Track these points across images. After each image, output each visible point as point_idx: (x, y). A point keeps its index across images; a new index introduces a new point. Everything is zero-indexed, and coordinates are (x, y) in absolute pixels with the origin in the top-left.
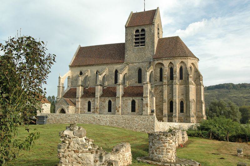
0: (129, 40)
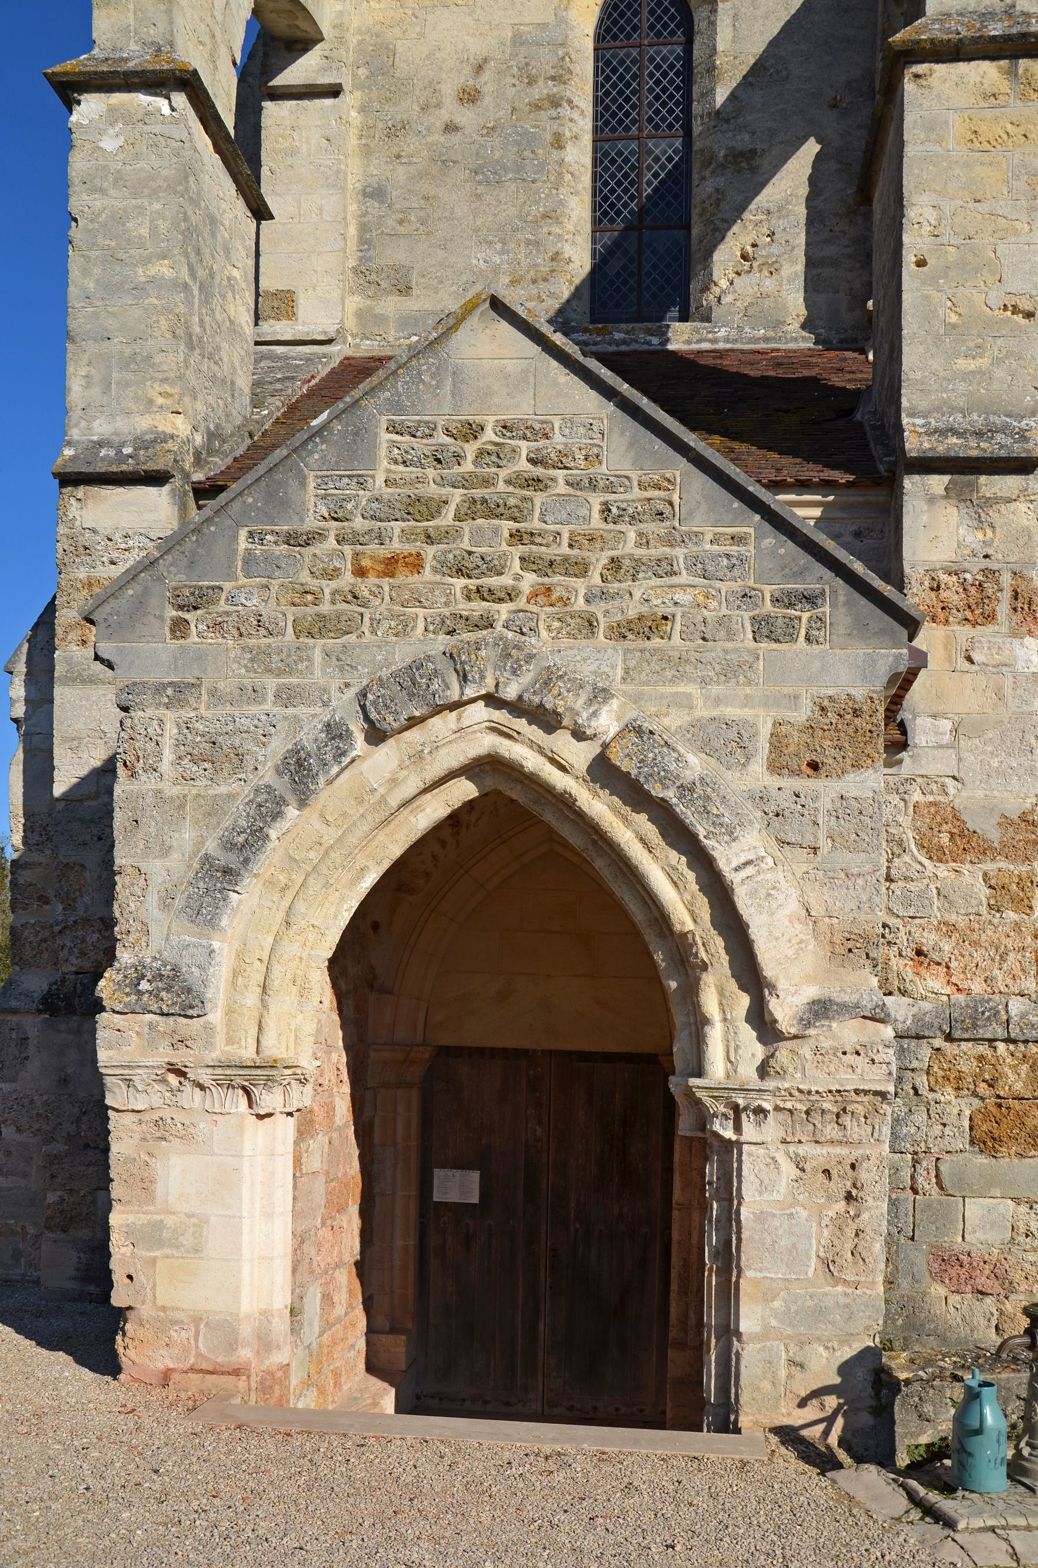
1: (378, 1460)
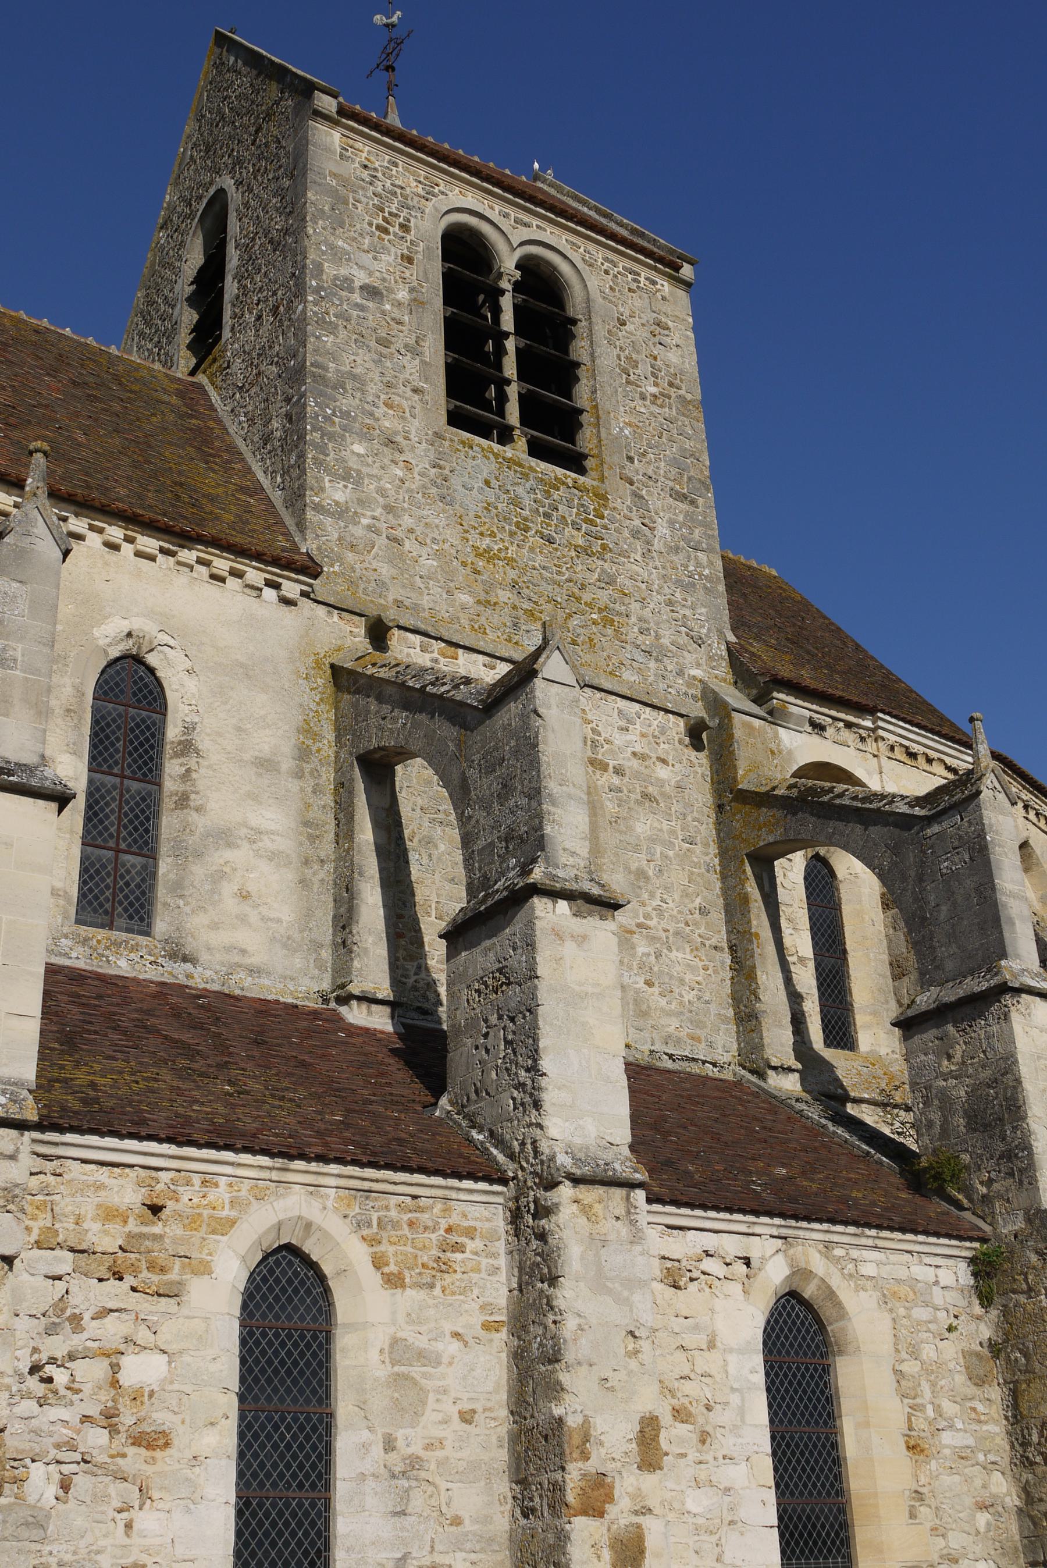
0: (371, 292)
1: (616, 780)
